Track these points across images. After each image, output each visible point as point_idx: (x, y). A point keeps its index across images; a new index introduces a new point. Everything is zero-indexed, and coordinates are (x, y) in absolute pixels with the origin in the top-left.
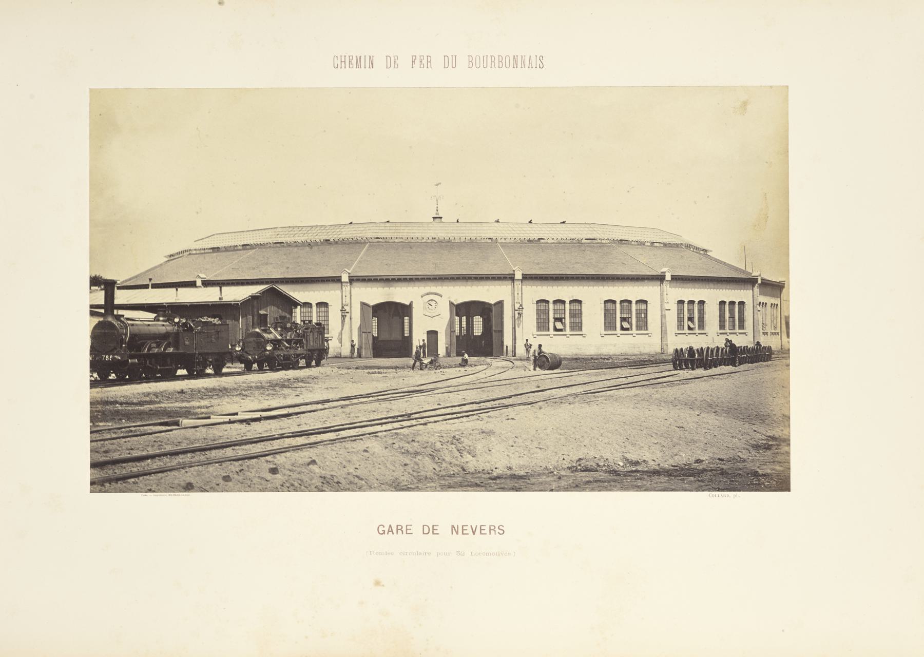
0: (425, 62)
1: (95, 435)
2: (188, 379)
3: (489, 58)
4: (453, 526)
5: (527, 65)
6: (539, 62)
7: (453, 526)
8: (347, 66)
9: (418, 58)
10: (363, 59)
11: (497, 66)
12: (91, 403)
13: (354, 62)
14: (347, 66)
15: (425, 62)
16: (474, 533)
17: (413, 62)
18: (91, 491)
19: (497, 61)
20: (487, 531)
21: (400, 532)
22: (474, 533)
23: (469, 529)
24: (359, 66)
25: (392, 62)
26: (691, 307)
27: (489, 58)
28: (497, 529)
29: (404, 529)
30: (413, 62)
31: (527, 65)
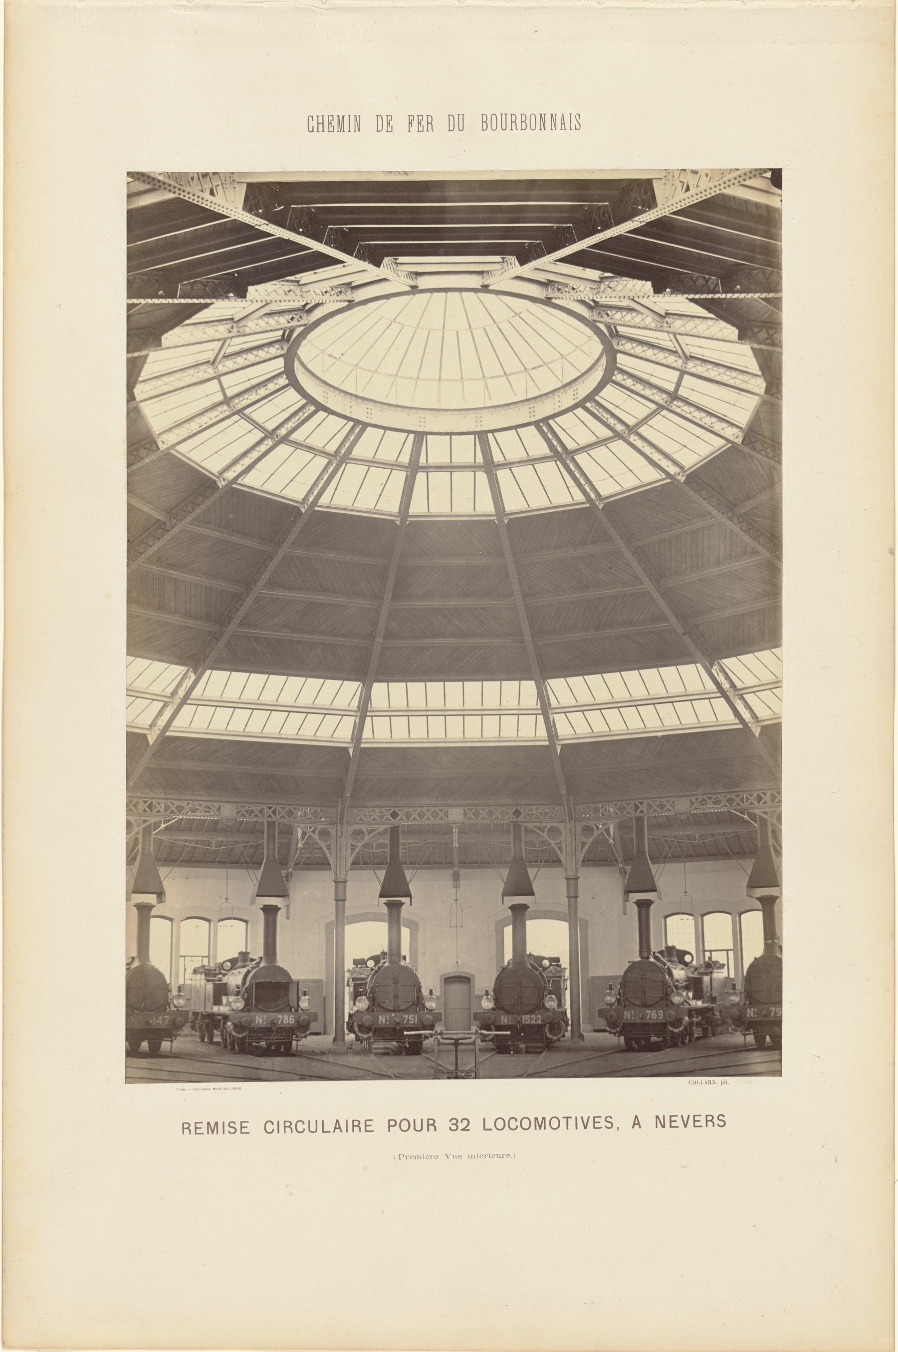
0: (424, 123)
2: (544, 304)
3: (509, 117)
4: (657, 1117)
6: (574, 122)
7: (657, 1117)
8: (326, 129)
9: (416, 118)
10: (346, 119)
11: (519, 127)
12: (138, 222)
14: (326, 129)
15: (424, 123)
16: (686, 1126)
17: (410, 123)
18: (129, 1079)
19: (519, 122)
20: (703, 1122)
22: (686, 1126)
23: (679, 1119)
24: (341, 129)
25: (385, 123)
27: (509, 117)
28: (716, 1121)
30: (410, 123)
31: (559, 127)
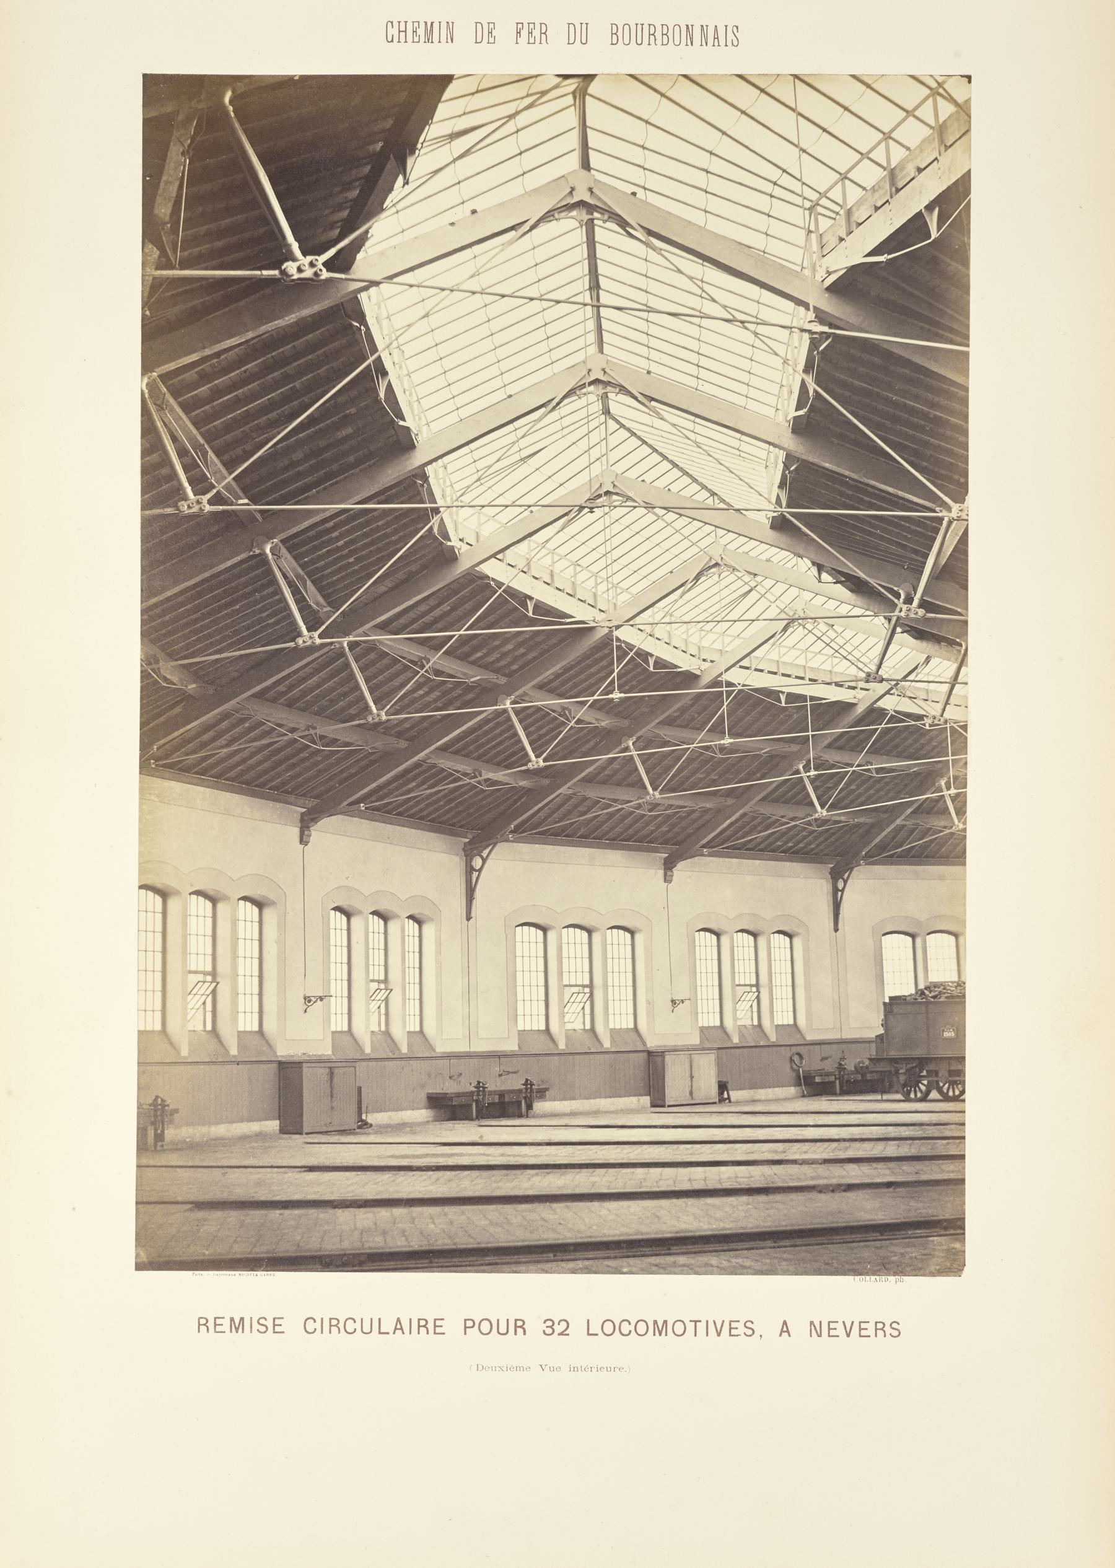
0: (536, 33)
1: (953, 1151)
3: (646, 28)
4: (812, 1323)
5: (710, 42)
6: (730, 36)
7: (812, 1323)
9: (526, 25)
10: (436, 26)
11: (659, 42)
13: (421, 31)
14: (409, 39)
15: (536, 33)
19: (658, 34)
20: (871, 1331)
21: (423, 1330)
23: (840, 1326)
26: (187, 460)
27: (646, 28)
28: (887, 1329)
29: (430, 1326)
30: (518, 33)
31: (710, 42)
